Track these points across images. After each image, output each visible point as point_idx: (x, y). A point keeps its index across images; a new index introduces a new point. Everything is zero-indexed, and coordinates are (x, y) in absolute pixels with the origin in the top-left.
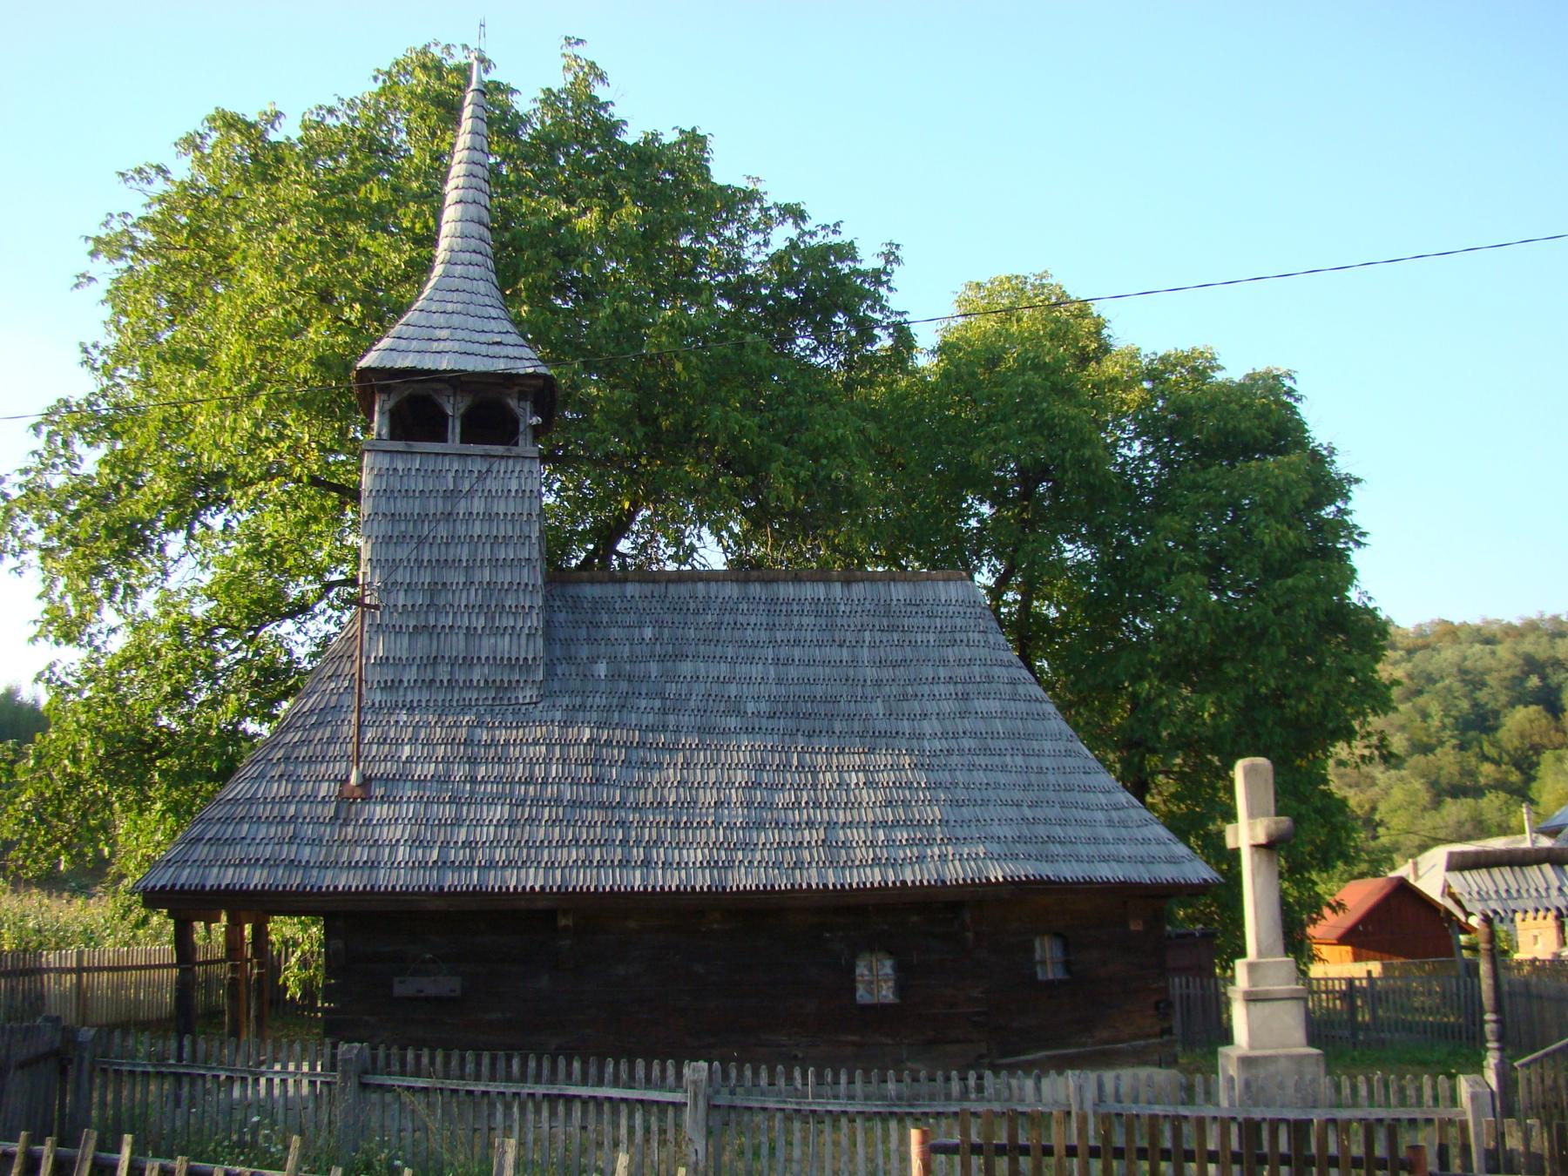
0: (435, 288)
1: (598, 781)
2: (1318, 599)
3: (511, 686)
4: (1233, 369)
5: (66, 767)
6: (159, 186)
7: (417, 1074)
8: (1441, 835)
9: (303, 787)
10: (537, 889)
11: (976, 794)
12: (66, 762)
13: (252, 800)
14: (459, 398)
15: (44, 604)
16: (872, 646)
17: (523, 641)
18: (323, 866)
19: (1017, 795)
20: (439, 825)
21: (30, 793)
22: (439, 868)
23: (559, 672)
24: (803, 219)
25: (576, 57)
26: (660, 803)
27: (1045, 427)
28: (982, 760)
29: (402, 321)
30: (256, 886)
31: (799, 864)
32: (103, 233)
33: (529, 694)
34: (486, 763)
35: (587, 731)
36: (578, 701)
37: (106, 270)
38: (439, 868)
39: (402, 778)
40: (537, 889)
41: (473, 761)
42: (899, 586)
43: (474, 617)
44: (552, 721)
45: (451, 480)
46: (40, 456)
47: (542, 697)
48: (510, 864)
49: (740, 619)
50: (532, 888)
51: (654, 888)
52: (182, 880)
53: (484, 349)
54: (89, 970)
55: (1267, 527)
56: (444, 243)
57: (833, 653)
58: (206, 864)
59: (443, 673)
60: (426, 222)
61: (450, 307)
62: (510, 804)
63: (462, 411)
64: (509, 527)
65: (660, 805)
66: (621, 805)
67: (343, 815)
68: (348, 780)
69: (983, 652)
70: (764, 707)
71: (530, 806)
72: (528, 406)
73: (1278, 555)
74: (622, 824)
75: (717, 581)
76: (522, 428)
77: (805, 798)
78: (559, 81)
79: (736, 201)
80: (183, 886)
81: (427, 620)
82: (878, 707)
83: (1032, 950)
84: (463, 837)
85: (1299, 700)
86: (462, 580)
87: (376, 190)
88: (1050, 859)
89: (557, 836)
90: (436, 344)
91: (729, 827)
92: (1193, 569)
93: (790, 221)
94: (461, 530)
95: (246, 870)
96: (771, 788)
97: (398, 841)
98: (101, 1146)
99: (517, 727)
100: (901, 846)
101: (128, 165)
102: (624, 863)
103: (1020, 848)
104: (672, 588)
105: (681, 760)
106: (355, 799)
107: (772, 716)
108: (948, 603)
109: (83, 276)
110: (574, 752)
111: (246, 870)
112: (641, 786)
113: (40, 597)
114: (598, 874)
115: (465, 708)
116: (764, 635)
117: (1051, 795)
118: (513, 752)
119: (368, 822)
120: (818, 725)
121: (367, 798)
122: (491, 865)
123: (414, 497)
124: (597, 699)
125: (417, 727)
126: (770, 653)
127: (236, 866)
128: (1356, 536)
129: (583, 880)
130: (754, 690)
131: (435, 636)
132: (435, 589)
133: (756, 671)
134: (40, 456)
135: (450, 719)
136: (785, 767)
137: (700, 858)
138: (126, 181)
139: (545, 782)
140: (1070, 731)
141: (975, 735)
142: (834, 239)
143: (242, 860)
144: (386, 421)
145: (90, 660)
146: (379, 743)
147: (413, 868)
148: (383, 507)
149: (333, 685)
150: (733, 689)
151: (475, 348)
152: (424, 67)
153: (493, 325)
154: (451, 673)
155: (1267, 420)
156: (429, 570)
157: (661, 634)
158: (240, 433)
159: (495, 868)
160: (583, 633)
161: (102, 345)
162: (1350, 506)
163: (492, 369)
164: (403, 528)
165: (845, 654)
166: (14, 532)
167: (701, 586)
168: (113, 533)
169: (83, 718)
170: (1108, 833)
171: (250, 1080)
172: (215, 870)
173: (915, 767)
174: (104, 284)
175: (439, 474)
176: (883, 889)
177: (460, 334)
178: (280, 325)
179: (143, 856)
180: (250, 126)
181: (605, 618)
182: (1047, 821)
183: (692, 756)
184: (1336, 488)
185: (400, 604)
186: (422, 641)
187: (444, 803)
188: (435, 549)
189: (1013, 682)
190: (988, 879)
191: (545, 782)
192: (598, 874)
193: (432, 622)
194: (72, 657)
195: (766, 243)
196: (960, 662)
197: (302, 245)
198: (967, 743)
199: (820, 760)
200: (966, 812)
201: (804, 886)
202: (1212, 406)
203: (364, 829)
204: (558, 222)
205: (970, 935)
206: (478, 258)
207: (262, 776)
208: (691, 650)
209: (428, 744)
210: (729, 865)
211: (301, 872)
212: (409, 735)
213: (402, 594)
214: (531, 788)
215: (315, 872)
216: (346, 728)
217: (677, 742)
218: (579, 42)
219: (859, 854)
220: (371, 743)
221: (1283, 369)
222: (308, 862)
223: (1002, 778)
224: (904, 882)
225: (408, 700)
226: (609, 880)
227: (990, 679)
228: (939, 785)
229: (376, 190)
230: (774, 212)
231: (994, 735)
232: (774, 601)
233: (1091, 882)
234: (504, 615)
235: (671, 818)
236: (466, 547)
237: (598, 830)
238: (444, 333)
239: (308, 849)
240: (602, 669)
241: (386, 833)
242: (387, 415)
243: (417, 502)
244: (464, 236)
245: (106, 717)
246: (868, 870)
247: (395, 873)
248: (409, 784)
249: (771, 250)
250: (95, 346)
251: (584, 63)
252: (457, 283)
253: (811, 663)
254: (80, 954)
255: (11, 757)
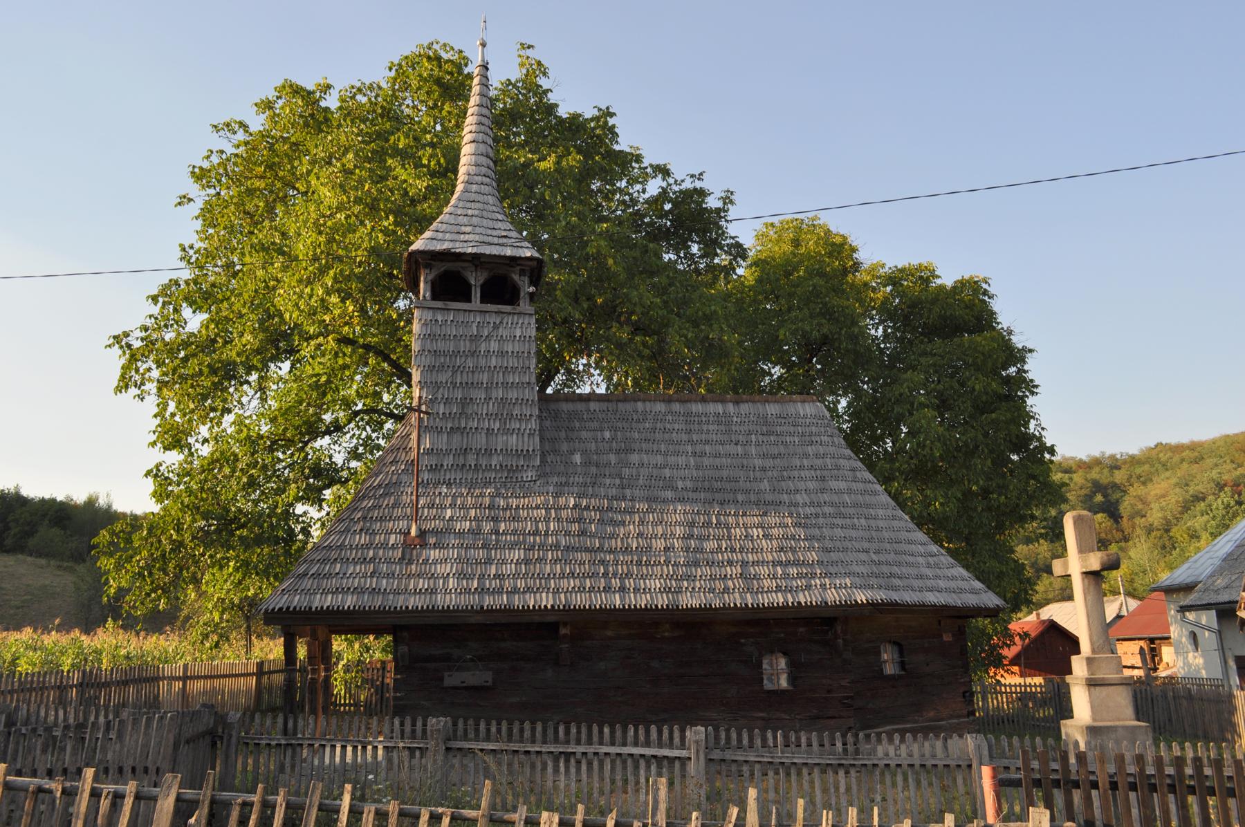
0: (459, 199)
1: (583, 533)
2: (1012, 427)
3: (518, 469)
4: (947, 278)
5: (172, 535)
6: (241, 136)
7: (488, 739)
8: (1050, 596)
9: (378, 537)
10: (549, 607)
11: (838, 544)
12: (172, 532)
13: (341, 547)
14: (479, 274)
15: (158, 421)
16: (758, 445)
17: (526, 439)
18: (397, 593)
19: (866, 545)
20: (476, 563)
21: (145, 553)
22: (479, 593)
23: (549, 460)
24: (669, 175)
25: (528, 58)
26: (626, 548)
27: (828, 313)
28: (839, 521)
29: (438, 220)
30: (349, 607)
31: (726, 590)
32: (206, 165)
33: (530, 474)
34: (505, 521)
35: (572, 499)
36: (564, 479)
37: (201, 196)
38: (479, 593)
39: (448, 531)
40: (549, 607)
41: (495, 520)
42: (771, 405)
43: (492, 422)
44: (548, 493)
45: (475, 328)
46: (156, 318)
47: (539, 477)
48: (528, 590)
49: (668, 426)
50: (546, 606)
51: (629, 606)
52: (295, 603)
53: (496, 240)
54: (191, 678)
55: (977, 379)
56: (462, 170)
57: (731, 449)
58: (310, 592)
59: (471, 460)
60: (438, 161)
61: (470, 212)
62: (524, 549)
63: (481, 282)
64: (515, 360)
65: (627, 550)
66: (600, 549)
67: (408, 557)
68: (409, 533)
69: (832, 449)
70: (689, 484)
71: (538, 550)
72: (526, 280)
73: (984, 398)
74: (602, 562)
75: (650, 401)
76: (522, 294)
77: (724, 546)
78: (516, 74)
79: (625, 161)
80: (295, 608)
81: (459, 423)
82: (765, 485)
83: (878, 654)
84: (493, 571)
85: (1000, 495)
86: (483, 396)
87: (402, 138)
88: (895, 589)
89: (559, 571)
90: (462, 236)
91: (676, 565)
92: (928, 407)
93: (660, 176)
94: (483, 362)
95: (340, 596)
96: (701, 538)
97: (448, 574)
98: (266, 791)
99: (524, 497)
100: (793, 578)
101: (221, 120)
102: (607, 589)
103: (873, 581)
104: (620, 405)
105: (637, 519)
106: (415, 546)
107: (695, 490)
108: (805, 417)
109: (185, 197)
110: (564, 514)
111: (340, 596)
112: (613, 536)
113: (155, 416)
114: (590, 596)
115: (487, 484)
116: (684, 437)
117: (888, 546)
118: (523, 514)
119: (426, 561)
120: (727, 496)
121: (424, 545)
122: (515, 591)
123: (449, 339)
124: (576, 479)
125: (454, 496)
126: (689, 449)
127: (333, 593)
128: (1031, 387)
129: (580, 600)
130: (682, 473)
131: (465, 435)
132: (465, 402)
133: (681, 460)
134: (156, 318)
135: (477, 491)
136: (708, 524)
137: (658, 586)
138: (218, 131)
139: (546, 534)
140: (893, 503)
141: (832, 504)
142: (698, 185)
143: (337, 589)
144: (429, 288)
145: (186, 462)
146: (428, 507)
147: (461, 593)
148: (428, 346)
149: (393, 468)
150: (667, 472)
151: (490, 239)
152: (429, 58)
153: (500, 225)
154: (477, 459)
155: (972, 310)
156: (460, 390)
157: (616, 435)
158: (315, 298)
159: (518, 593)
160: (563, 434)
161: (197, 246)
162: (1026, 367)
163: (503, 254)
164: (442, 360)
165: (740, 449)
166: (137, 371)
167: (640, 404)
168: (213, 371)
169: (186, 500)
170: (928, 572)
171: (360, 748)
172: (318, 596)
173: (795, 525)
174: (199, 204)
175: (467, 324)
176: (785, 607)
177: (478, 230)
178: (343, 225)
179: (218, 599)
180: (310, 93)
181: (577, 425)
182: (888, 563)
183: (644, 516)
184: (1017, 356)
185: (441, 412)
186: (456, 438)
187: (478, 548)
188: (465, 375)
189: (853, 470)
190: (856, 601)
191: (546, 534)
192: (590, 596)
193: (463, 426)
194: (174, 458)
195: (644, 191)
196: (817, 456)
197: (357, 171)
198: (827, 510)
199: (731, 520)
200: (834, 556)
201: (732, 605)
202: (935, 301)
203: (423, 567)
204: (527, 165)
205: (840, 641)
206: (487, 180)
207: (347, 530)
208: (637, 446)
209: (463, 508)
210: (679, 591)
211: (381, 597)
212: (449, 502)
213: (442, 406)
214: (538, 538)
215: (391, 597)
216: (404, 497)
217: (634, 507)
218: (529, 47)
219: (766, 583)
220: (423, 508)
221: (981, 276)
222: (385, 590)
223: (854, 533)
224: (799, 603)
225: (447, 478)
226: (599, 600)
227: (838, 468)
228: (813, 538)
229: (402, 138)
230: (649, 170)
231: (845, 505)
232: (689, 414)
233: (924, 605)
234: (513, 421)
235: (635, 558)
236: (486, 374)
237: (587, 566)
238: (468, 229)
239: (384, 581)
240: (577, 458)
241: (439, 569)
242: (429, 284)
243: (452, 343)
244: (477, 165)
245: (202, 499)
246: (774, 594)
247: (448, 597)
248: (452, 536)
249: (647, 196)
250: (191, 247)
251: (533, 62)
252: (473, 197)
253: (717, 455)
254: (185, 666)
255: (129, 529)
